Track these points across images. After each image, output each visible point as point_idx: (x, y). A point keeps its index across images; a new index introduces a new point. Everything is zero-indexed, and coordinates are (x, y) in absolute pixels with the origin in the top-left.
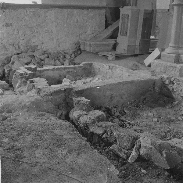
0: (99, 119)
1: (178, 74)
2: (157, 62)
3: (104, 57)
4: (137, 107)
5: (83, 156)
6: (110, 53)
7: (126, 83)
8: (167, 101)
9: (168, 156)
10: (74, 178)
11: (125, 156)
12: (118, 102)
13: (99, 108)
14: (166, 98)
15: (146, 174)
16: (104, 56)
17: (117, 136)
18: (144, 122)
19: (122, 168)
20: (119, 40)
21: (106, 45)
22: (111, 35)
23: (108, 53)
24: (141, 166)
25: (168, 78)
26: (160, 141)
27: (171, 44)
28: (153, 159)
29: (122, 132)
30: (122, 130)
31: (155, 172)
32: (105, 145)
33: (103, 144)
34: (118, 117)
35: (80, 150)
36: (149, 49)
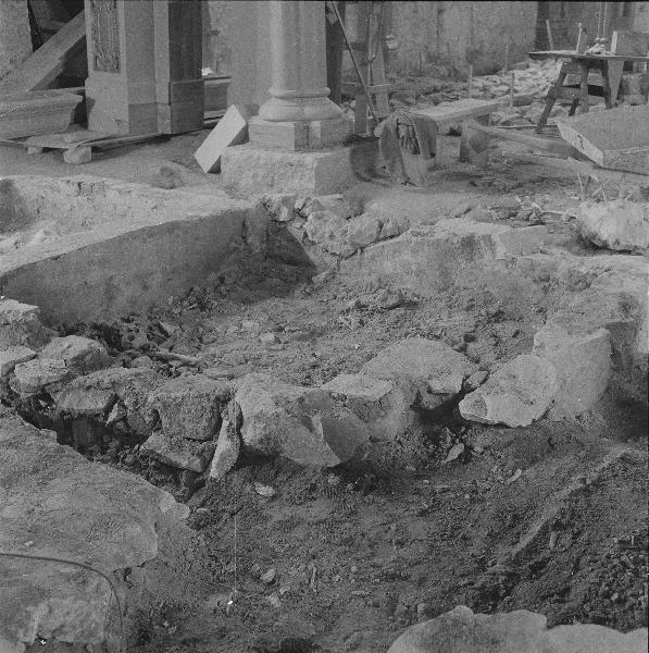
0: (82, 364)
1: (312, 186)
2: (238, 151)
3: (48, 156)
4: (203, 308)
5: (61, 484)
6: (69, 138)
7: (150, 233)
8: (292, 276)
9: (328, 429)
10: (47, 555)
11: (196, 464)
12: (133, 302)
13: (68, 331)
14: (287, 269)
15: (274, 498)
16: (46, 150)
17: (159, 405)
18: (234, 350)
19: (196, 500)
20: (92, 87)
21: (47, 111)
22: (61, 70)
23: (62, 139)
24: (252, 479)
25: (285, 201)
26: (301, 391)
27: (275, 91)
28: (287, 450)
29: (173, 389)
30: (171, 383)
31: (297, 485)
32: (122, 444)
33: (115, 444)
34: (144, 349)
35: (42, 472)
36: (202, 114)
